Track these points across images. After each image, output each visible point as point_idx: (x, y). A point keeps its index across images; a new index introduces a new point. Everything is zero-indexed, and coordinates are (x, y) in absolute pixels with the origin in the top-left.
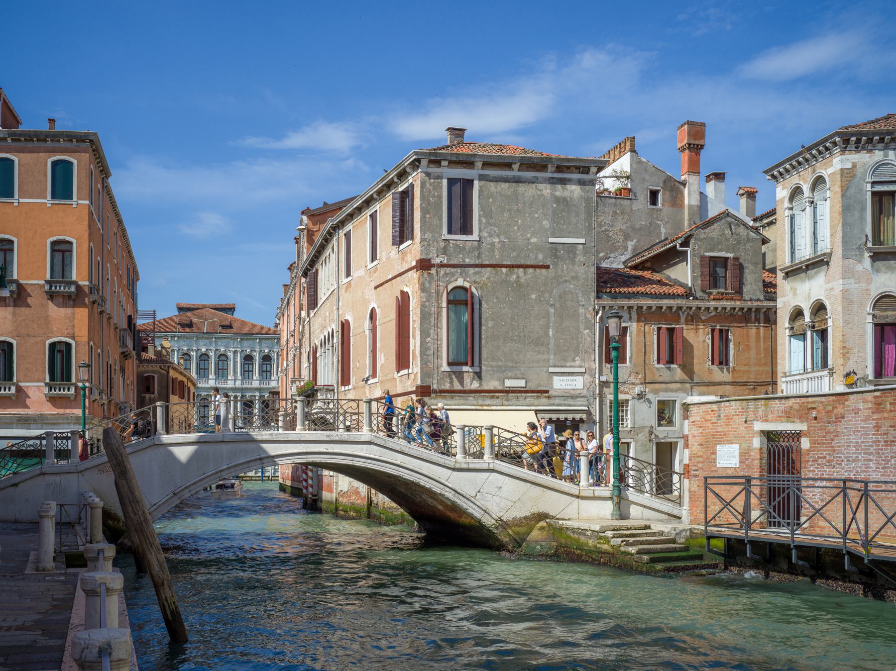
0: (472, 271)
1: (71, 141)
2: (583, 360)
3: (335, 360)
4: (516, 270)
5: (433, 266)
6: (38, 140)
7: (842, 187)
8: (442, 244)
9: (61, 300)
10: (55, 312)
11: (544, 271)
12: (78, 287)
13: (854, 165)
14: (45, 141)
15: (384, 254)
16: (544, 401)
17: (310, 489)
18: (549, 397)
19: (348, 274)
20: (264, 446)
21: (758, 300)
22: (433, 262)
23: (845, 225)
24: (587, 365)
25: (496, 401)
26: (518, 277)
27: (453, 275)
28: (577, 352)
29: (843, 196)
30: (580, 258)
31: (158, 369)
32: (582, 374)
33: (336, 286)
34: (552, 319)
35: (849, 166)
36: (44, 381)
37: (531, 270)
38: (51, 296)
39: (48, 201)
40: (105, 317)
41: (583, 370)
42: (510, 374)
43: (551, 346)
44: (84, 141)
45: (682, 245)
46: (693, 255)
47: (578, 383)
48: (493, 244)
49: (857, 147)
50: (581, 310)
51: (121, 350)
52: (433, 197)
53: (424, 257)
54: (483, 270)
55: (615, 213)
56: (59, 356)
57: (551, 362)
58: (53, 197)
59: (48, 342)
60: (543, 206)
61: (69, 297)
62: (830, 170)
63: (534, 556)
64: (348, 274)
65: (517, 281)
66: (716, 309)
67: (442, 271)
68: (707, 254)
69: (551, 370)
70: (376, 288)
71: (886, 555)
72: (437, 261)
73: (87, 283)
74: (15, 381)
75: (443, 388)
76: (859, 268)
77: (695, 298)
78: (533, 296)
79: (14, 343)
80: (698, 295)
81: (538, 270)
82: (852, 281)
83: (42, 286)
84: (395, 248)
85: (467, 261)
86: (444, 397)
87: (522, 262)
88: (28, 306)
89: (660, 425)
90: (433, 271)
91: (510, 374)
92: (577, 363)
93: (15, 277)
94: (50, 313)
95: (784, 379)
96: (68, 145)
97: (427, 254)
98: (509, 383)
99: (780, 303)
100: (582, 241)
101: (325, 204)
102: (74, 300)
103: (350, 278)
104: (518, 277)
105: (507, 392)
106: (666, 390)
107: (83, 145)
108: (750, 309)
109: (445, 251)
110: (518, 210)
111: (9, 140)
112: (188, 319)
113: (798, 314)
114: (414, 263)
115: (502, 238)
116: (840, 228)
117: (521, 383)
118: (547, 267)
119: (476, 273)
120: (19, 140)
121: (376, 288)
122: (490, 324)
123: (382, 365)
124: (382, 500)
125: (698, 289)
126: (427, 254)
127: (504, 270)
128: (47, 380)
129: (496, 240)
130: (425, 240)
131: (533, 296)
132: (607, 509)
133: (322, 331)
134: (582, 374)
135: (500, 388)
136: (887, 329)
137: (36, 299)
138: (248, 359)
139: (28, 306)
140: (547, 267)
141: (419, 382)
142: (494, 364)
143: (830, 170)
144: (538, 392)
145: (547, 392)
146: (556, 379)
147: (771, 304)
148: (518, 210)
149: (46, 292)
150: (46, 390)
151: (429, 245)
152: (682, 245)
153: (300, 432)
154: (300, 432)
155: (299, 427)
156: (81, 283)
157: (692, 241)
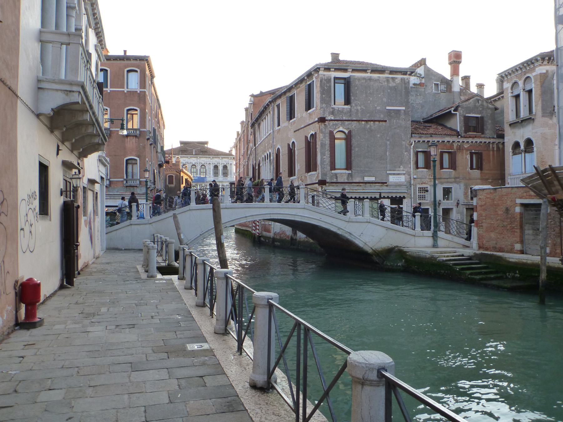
0: (347, 123)
2: (404, 167)
3: (272, 168)
4: (369, 123)
5: (327, 120)
7: (540, 82)
8: (331, 110)
11: (384, 123)
13: (547, 71)
15: (299, 115)
16: (385, 188)
17: (258, 231)
18: (387, 186)
19: (279, 125)
21: (493, 138)
22: (327, 118)
23: (543, 101)
24: (406, 170)
25: (360, 188)
26: (371, 126)
27: (336, 125)
28: (401, 164)
29: (541, 86)
30: (403, 116)
32: (404, 174)
33: (272, 131)
34: (389, 147)
35: (545, 71)
37: (377, 123)
41: (404, 172)
42: (367, 174)
43: (388, 160)
45: (454, 111)
46: (459, 116)
47: (402, 179)
48: (357, 110)
49: (548, 62)
50: (404, 143)
52: (327, 86)
53: (322, 116)
54: (353, 122)
55: (417, 95)
57: (388, 168)
60: (383, 91)
62: (534, 74)
63: (121, 250)
64: (279, 125)
65: (370, 128)
66: (472, 142)
67: (331, 123)
68: (467, 115)
69: (388, 172)
70: (295, 132)
71: (96, 239)
72: (329, 118)
75: (333, 181)
76: (550, 122)
77: (461, 137)
78: (379, 136)
80: (463, 135)
81: (381, 123)
82: (547, 128)
84: (305, 112)
85: (344, 118)
86: (333, 186)
87: (373, 119)
89: (444, 200)
90: (327, 123)
91: (367, 174)
92: (402, 169)
95: (509, 177)
97: (324, 115)
98: (367, 179)
99: (506, 139)
100: (404, 108)
103: (279, 127)
104: (371, 126)
105: (366, 183)
106: (448, 182)
108: (489, 142)
109: (333, 113)
110: (370, 93)
112: (186, 148)
113: (516, 145)
114: (316, 119)
115: (362, 107)
116: (540, 102)
117: (373, 179)
118: (386, 121)
119: (349, 124)
121: (295, 132)
122: (357, 149)
123: (298, 170)
124: (301, 236)
125: (462, 132)
126: (324, 115)
127: (363, 123)
129: (359, 108)
130: (323, 108)
131: (379, 136)
132: (430, 241)
133: (263, 153)
134: (404, 174)
135: (362, 181)
136: (419, 154)
138: (216, 167)
140: (386, 121)
141: (320, 178)
142: (359, 169)
143: (534, 74)
144: (382, 183)
145: (386, 183)
146: (390, 177)
147: (501, 140)
148: (370, 93)
151: (324, 110)
152: (454, 111)
157: (460, 108)
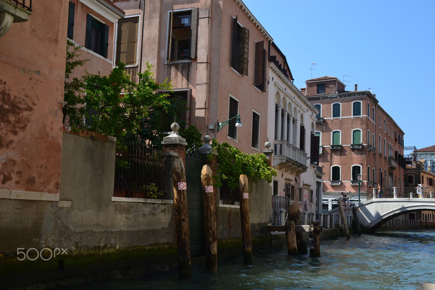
1: (360, 95)
6: (348, 96)
9: (356, 151)
10: (355, 156)
12: (363, 146)
14: (351, 96)
20: (366, 206)
31: (415, 172)
36: (330, 180)
38: (353, 150)
39: (352, 116)
40: (377, 156)
44: (365, 94)
51: (389, 166)
56: (356, 170)
58: (354, 115)
59: (352, 166)
61: (359, 150)
73: (366, 145)
74: (340, 180)
79: (340, 167)
83: (350, 147)
88: (346, 155)
93: (340, 144)
94: (353, 156)
96: (359, 96)
101: (375, 95)
102: (361, 151)
107: (364, 96)
111: (338, 97)
120: (342, 97)
128: (352, 180)
137: (348, 151)
139: (346, 155)
149: (351, 149)
150: (351, 183)
153: (421, 198)
154: (421, 198)
155: (394, 197)
156: (364, 145)
